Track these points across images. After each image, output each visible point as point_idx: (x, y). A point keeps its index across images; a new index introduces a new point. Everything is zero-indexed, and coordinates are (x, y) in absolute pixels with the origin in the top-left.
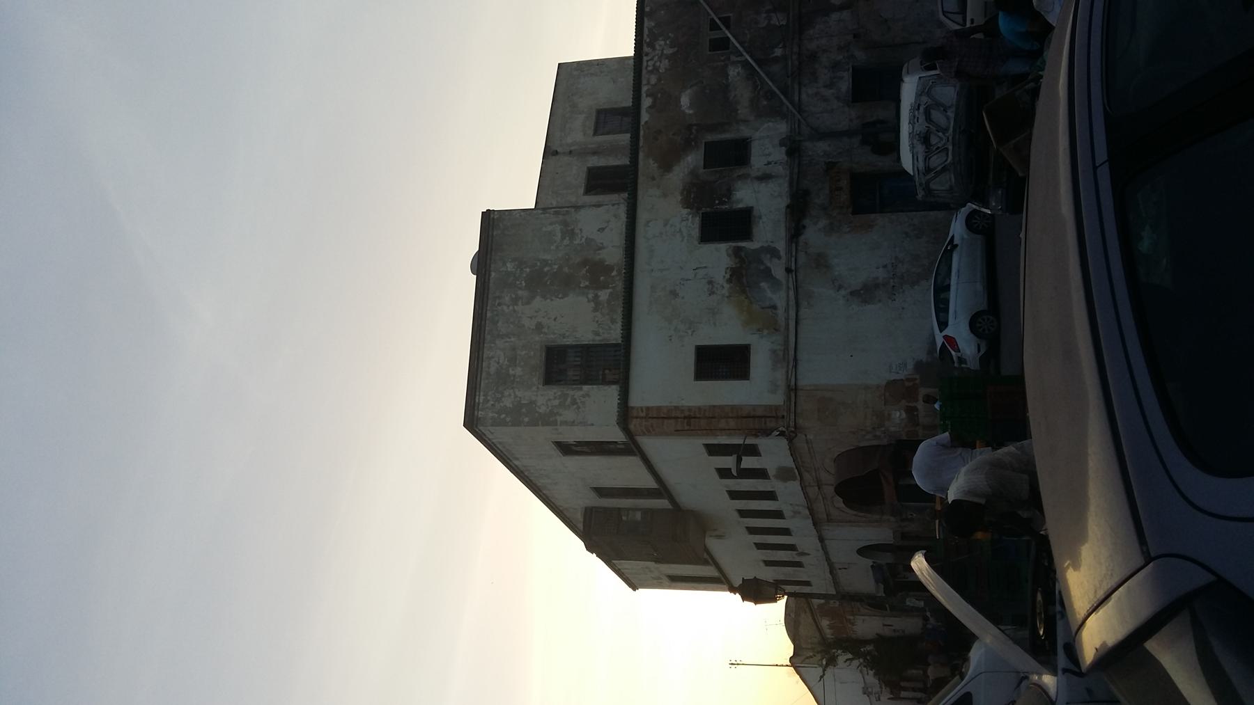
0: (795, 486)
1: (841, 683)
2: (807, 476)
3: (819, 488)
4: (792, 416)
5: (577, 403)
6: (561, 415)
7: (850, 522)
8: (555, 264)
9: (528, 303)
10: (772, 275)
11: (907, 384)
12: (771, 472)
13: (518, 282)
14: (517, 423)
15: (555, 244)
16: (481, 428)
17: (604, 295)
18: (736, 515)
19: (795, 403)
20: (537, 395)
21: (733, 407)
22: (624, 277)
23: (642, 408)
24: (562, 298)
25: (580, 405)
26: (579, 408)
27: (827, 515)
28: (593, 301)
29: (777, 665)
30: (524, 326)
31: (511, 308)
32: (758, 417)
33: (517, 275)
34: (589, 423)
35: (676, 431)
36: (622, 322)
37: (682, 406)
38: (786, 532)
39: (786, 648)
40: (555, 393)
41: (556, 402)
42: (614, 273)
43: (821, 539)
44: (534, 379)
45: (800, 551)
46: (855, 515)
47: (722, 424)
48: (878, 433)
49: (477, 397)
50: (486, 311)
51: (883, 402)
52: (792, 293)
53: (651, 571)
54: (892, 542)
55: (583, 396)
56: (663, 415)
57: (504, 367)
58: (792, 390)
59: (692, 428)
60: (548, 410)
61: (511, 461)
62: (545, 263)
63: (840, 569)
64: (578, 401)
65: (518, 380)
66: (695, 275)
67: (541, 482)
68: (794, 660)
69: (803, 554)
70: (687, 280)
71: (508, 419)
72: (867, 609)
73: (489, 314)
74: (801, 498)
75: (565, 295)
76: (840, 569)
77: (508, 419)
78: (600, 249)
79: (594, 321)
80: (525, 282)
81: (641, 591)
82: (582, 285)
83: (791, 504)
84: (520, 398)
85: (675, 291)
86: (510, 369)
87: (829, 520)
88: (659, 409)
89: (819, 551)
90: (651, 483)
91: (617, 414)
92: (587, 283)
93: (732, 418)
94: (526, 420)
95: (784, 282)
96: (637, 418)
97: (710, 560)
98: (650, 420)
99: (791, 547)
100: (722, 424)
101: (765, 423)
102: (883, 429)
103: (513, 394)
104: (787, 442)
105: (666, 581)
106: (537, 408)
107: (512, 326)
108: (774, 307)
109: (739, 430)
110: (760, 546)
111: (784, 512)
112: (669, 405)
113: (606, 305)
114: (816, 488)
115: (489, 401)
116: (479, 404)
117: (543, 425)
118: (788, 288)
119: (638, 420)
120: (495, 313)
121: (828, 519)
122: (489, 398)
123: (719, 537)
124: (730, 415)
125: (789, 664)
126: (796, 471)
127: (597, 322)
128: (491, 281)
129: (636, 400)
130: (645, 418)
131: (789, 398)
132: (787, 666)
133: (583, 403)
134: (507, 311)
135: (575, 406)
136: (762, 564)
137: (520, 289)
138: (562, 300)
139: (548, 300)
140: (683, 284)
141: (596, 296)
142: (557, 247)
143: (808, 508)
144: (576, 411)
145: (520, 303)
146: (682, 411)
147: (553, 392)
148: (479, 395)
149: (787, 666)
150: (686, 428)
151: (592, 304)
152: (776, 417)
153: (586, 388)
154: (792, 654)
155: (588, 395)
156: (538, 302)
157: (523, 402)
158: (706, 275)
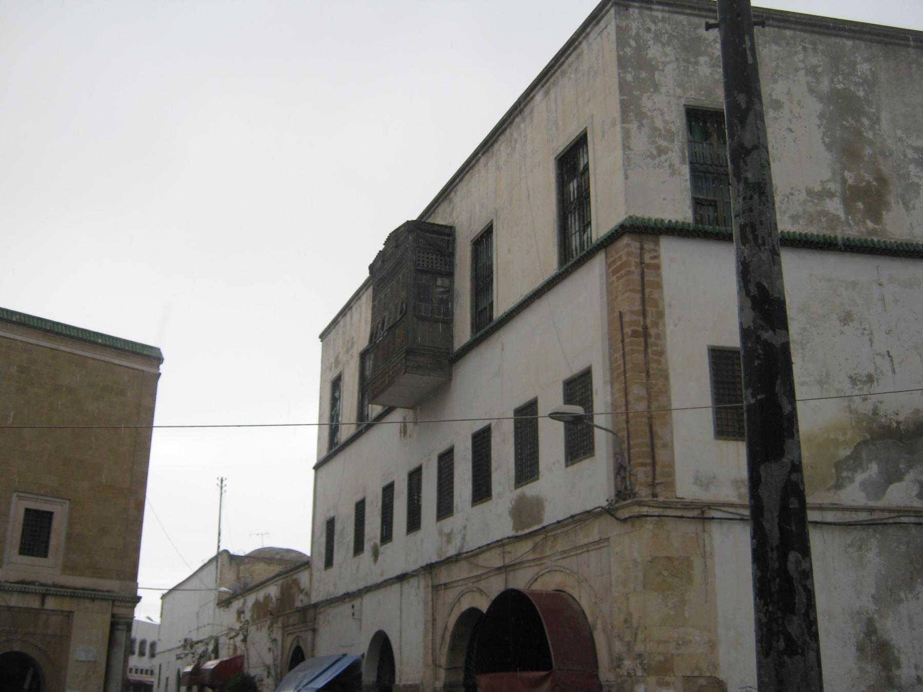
0: (504, 528)
1: (198, 613)
2: (527, 545)
3: (499, 568)
4: (656, 511)
5: (659, 156)
6: (639, 128)
7: (434, 620)
8: (874, 134)
9: (811, 91)
10: (891, 483)
12: (530, 489)
13: (841, 78)
14: (622, 63)
15: (904, 136)
16: (612, 11)
17: (835, 206)
18: (442, 447)
19: (682, 517)
20: (668, 95)
21: (667, 410)
22: (866, 240)
23: (656, 257)
24: (824, 142)
25: (657, 161)
26: (652, 157)
27: (445, 584)
28: (824, 188)
29: (219, 535)
30: (776, 82)
31: (801, 65)
32: (653, 456)
33: (852, 78)
34: (629, 172)
35: (621, 314)
36: (794, 233)
37: (664, 325)
38: (414, 523)
39: (241, 547)
40: (673, 122)
41: (659, 124)
42: (870, 224)
43: (402, 578)
44: (693, 93)
45: (381, 549)
46: (446, 628)
47: (637, 391)
48: (627, 663)
49: (660, 7)
50: (793, 29)
51: (689, 674)
52: (863, 516)
53: (348, 351)
54: (397, 682)
55: (671, 166)
56: (647, 291)
57: (710, 50)
59: (627, 340)
60: (645, 110)
61: (542, 86)
62: (875, 120)
63: (353, 607)
64: (663, 158)
65: (691, 69)
66: (879, 354)
67: (501, 148)
68: (225, 555)
69: (376, 554)
70: (871, 340)
71: (628, 50)
72: (291, 645)
73: (788, 33)
74: (473, 543)
75: (829, 147)
76: (353, 607)
77: (628, 50)
78: (906, 205)
79: (792, 189)
80: (844, 89)
81: (319, 344)
83: (465, 528)
84: (663, 70)
85: (852, 320)
86: (706, 58)
87: (436, 588)
88: (658, 286)
89: (382, 575)
90: (500, 309)
91: (646, 217)
92: (850, 182)
93: (649, 407)
94: (629, 77)
95: (880, 504)
96: (642, 249)
97: (365, 425)
98: (639, 270)
99: (386, 536)
100: (637, 391)
101: (643, 465)
102: (639, 673)
103: (668, 59)
104: (604, 504)
105: (332, 375)
106: (649, 94)
107: (774, 64)
108: (838, 486)
109: (627, 422)
110: (388, 491)
111: (450, 519)
112: (666, 303)
113: (819, 208)
114: (500, 564)
115: (656, 24)
116: (650, 9)
117: (622, 102)
118: (871, 510)
119: (639, 251)
120: (792, 42)
121: (437, 586)
122: (660, 24)
123: (404, 432)
124: (654, 405)
125: (221, 549)
126: (539, 527)
127: (792, 194)
128: (838, 40)
129: (670, 249)
130: (642, 263)
131: (688, 506)
132: (219, 547)
133: (660, 166)
134: (796, 59)
135: (655, 152)
136: (358, 498)
137: (832, 81)
138: (821, 141)
139: (818, 122)
140: (863, 334)
141: (831, 195)
142: (901, 140)
143: (459, 554)
144: (648, 154)
145: (809, 78)
146: (656, 324)
147: (677, 122)
148: (663, 11)
149: (219, 547)
150: (628, 330)
151: (818, 188)
152: (653, 485)
153: (686, 170)
154: (232, 552)
155: (673, 173)
156: (814, 106)
157: (657, 73)
158: (882, 372)
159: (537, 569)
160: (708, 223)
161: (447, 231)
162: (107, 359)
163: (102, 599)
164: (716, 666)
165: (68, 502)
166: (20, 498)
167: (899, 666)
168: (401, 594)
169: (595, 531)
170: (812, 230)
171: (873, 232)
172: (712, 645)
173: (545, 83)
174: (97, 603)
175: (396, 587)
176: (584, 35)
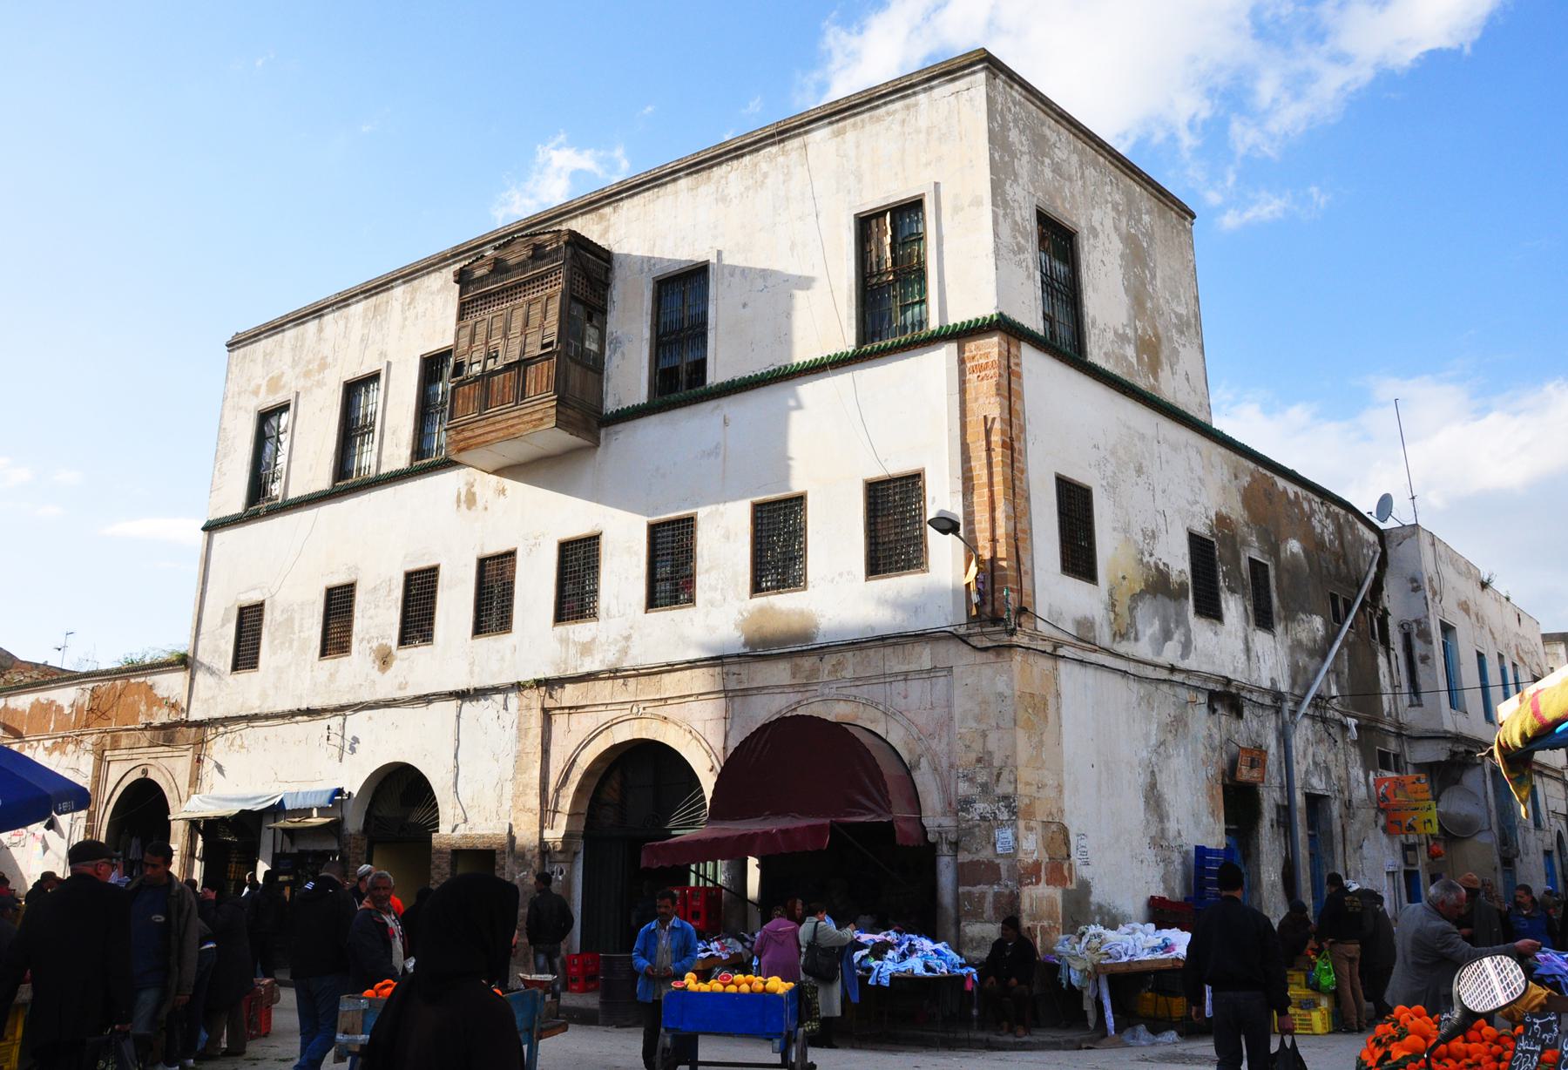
11: (1066, 866)
46: (572, 763)
49: (1020, 89)
58: (1055, 648)
61: (831, 123)
82: (1137, 322)
83: (628, 638)
116: (1011, 87)
148: (1020, 94)
153: (1038, 275)
159: (799, 697)
161: (605, 256)
164: (1061, 811)
167: (1168, 820)
169: (924, 657)
170: (1117, 371)
171: (1153, 387)
172: (1060, 788)
173: (837, 121)
175: (453, 704)
176: (926, 86)
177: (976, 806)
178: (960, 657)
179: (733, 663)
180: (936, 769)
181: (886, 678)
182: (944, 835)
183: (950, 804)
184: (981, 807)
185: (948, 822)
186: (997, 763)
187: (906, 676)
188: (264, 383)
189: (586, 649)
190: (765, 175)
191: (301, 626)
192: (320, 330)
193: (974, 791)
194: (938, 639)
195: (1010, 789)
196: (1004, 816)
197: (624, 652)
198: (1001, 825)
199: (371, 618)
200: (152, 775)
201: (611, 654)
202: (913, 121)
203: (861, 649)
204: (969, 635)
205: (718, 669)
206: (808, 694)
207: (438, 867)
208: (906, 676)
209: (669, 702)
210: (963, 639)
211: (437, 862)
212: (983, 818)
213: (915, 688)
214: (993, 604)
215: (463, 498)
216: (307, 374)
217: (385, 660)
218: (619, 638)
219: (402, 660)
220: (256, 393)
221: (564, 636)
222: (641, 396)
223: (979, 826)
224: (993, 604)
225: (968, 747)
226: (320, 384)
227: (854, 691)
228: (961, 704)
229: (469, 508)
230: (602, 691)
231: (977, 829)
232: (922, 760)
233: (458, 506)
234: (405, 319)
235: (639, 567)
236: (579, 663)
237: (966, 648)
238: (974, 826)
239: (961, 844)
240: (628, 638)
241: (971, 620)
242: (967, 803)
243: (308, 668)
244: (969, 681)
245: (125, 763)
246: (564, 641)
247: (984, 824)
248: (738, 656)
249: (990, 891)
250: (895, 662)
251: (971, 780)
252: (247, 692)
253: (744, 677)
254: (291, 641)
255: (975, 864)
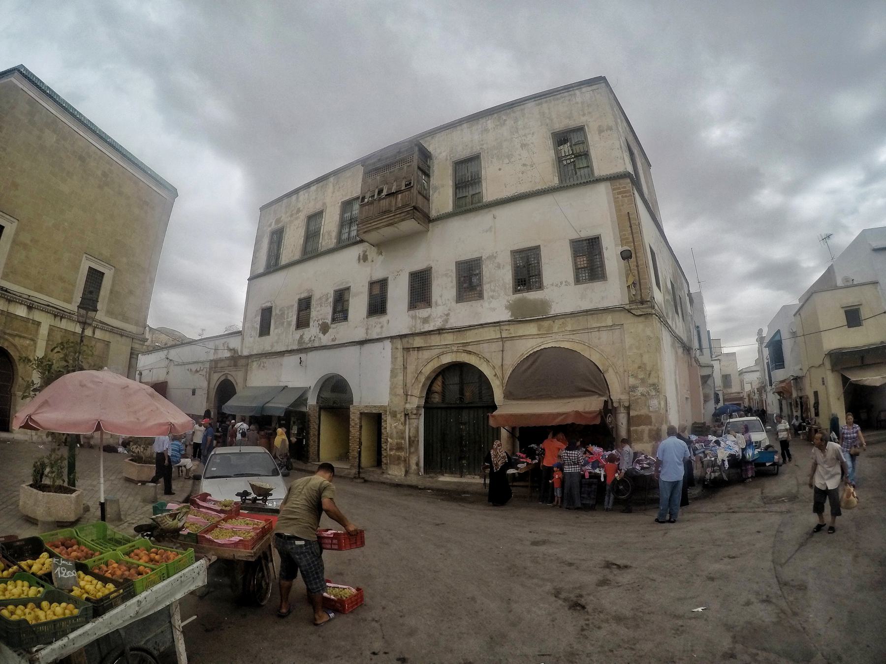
83: (448, 315)
159: (542, 340)
160: (359, 229)
162: (151, 185)
163: (127, 337)
165: (113, 269)
166: (87, 259)
168: (627, 142)
169: (609, 320)
174: (124, 338)
177: (639, 389)
178: (628, 321)
179: (506, 325)
180: (617, 373)
181: (589, 330)
182: (622, 404)
183: (625, 389)
184: (641, 389)
185: (624, 397)
186: (648, 369)
187: (599, 329)
188: (274, 221)
189: (426, 320)
190: (505, 120)
191: (288, 316)
192: (297, 198)
193: (637, 382)
194: (614, 311)
195: (656, 381)
196: (653, 393)
197: (446, 321)
198: (652, 397)
199: (318, 311)
200: (230, 378)
201: (439, 323)
202: (574, 100)
203: (575, 317)
204: (631, 309)
205: (498, 328)
206: (547, 339)
207: (353, 420)
208: (599, 329)
209: (471, 344)
210: (629, 311)
211: (353, 418)
212: (642, 395)
213: (605, 336)
214: (641, 295)
215: (361, 257)
216: (291, 216)
217: (324, 329)
218: (443, 315)
219: (333, 328)
220: (270, 225)
221: (414, 315)
222: (449, 208)
223: (640, 398)
224: (641, 295)
225: (633, 361)
226: (297, 218)
227: (572, 337)
228: (628, 341)
229: (364, 261)
230: (435, 340)
231: (640, 400)
232: (610, 368)
233: (359, 261)
234: (334, 189)
235: (452, 282)
236: (422, 327)
237: (629, 315)
238: (638, 399)
239: (631, 407)
240: (448, 315)
241: (631, 302)
242: (633, 388)
243: (291, 333)
244: (632, 331)
245: (219, 373)
246: (414, 317)
247: (643, 398)
248: (509, 321)
249: (646, 428)
250: (593, 322)
251: (636, 377)
252: (267, 344)
253: (512, 331)
254: (283, 323)
255: (638, 417)
